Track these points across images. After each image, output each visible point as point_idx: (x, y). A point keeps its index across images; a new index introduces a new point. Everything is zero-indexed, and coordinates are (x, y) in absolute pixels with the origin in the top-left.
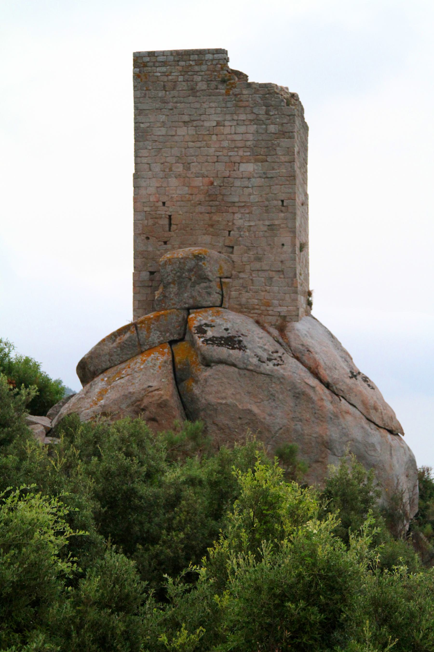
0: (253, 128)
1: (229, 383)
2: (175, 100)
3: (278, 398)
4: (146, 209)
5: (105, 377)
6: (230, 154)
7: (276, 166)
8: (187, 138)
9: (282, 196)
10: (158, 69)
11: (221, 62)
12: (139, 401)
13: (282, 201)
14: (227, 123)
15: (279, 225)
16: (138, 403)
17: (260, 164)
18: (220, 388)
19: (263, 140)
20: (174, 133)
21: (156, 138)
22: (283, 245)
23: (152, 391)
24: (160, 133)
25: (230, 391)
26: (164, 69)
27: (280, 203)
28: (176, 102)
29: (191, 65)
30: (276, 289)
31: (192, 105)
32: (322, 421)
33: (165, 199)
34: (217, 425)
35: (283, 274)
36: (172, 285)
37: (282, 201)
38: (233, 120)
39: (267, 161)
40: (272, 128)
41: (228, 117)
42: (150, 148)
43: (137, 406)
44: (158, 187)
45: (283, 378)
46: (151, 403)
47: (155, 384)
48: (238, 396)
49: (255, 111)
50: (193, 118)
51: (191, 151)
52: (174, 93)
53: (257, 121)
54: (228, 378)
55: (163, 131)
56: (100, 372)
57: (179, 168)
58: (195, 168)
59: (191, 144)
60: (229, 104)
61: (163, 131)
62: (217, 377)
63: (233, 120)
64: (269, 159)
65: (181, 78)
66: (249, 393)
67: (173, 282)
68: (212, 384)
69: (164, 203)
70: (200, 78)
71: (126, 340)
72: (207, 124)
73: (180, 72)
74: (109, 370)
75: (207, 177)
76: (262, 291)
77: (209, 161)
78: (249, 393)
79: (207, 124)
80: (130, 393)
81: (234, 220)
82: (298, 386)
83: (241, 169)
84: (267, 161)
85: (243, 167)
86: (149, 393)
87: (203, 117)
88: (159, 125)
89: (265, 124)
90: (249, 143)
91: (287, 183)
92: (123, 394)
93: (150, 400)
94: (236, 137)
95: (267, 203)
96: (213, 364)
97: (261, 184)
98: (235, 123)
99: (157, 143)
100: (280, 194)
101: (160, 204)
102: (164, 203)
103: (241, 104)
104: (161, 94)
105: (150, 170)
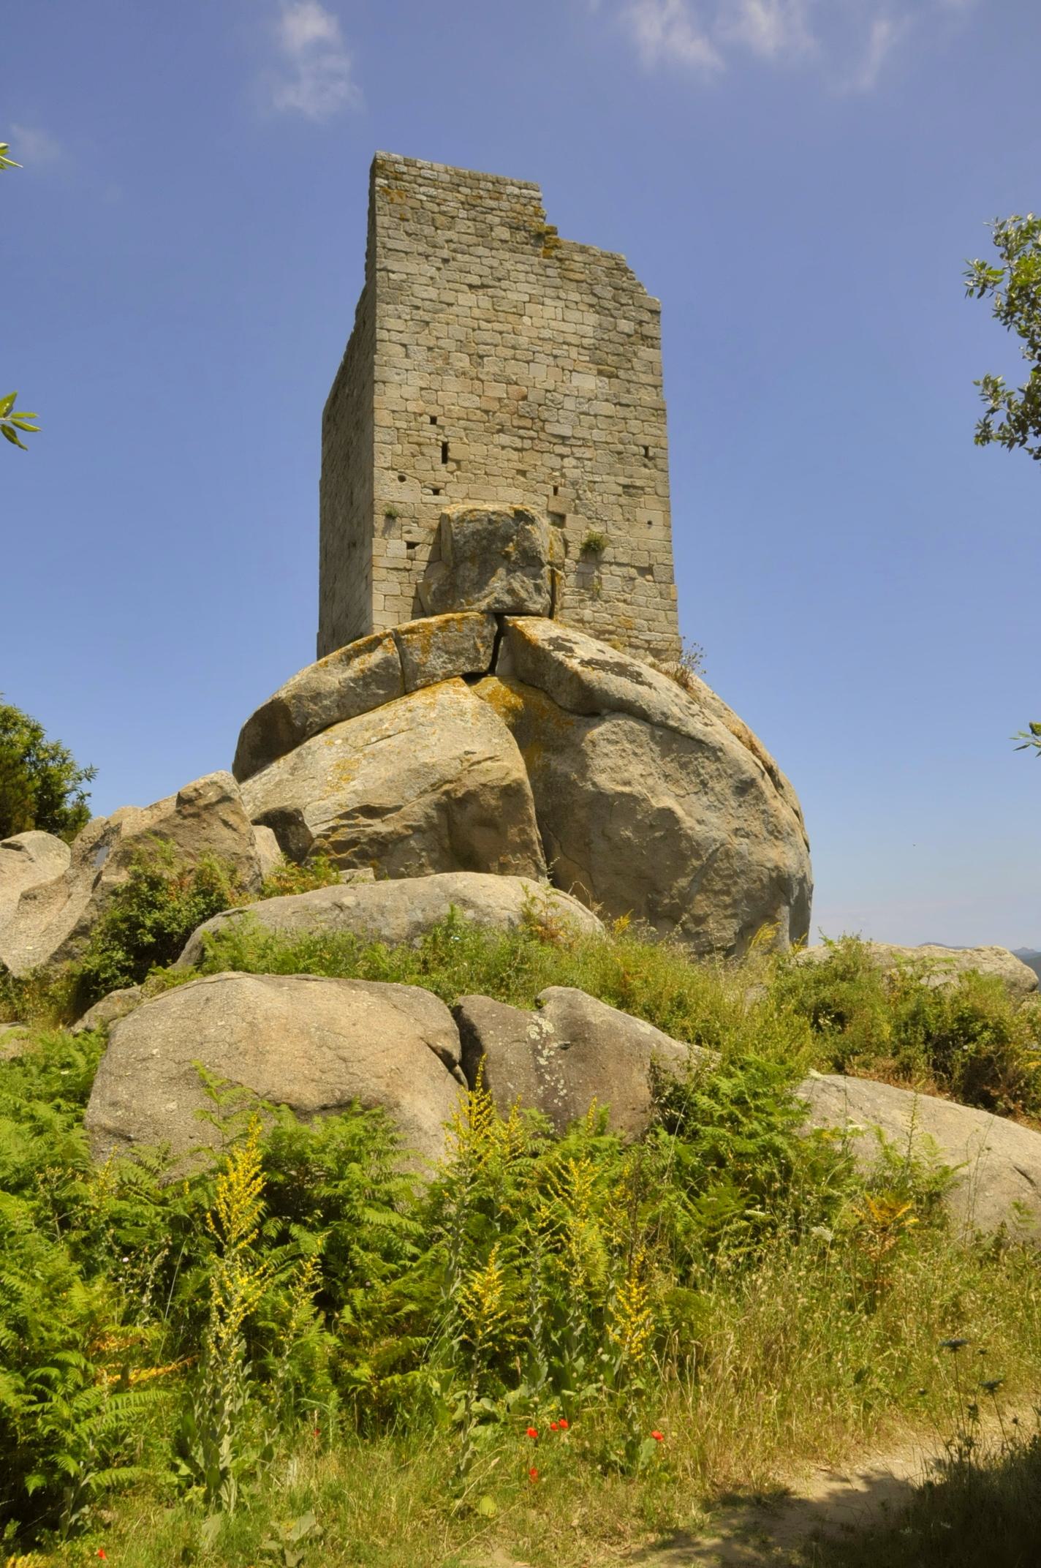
0: (592, 318)
1: (635, 754)
2: (453, 246)
3: (712, 789)
4: (398, 424)
5: (337, 737)
6: (555, 352)
7: (632, 387)
8: (476, 312)
9: (648, 441)
10: (422, 189)
11: (534, 203)
12: (451, 782)
13: (646, 448)
14: (547, 301)
15: (642, 488)
16: (447, 787)
17: (606, 380)
18: (620, 762)
19: (609, 341)
20: (452, 301)
21: (419, 303)
22: (650, 523)
23: (479, 762)
24: (425, 295)
25: (635, 770)
26: (432, 191)
27: (643, 451)
28: (454, 251)
29: (481, 198)
30: (642, 599)
31: (485, 261)
32: (776, 838)
33: (434, 411)
34: (609, 839)
35: (652, 574)
36: (469, 564)
37: (646, 448)
38: (558, 298)
39: (617, 377)
40: (625, 326)
41: (550, 292)
42: (408, 317)
43: (447, 793)
44: (422, 389)
45: (721, 750)
46: (484, 785)
47: (480, 749)
48: (650, 781)
49: (598, 289)
50: (486, 281)
51: (487, 336)
52: (450, 234)
53: (598, 309)
54: (632, 742)
55: (432, 293)
56: (317, 729)
57: (462, 361)
58: (491, 366)
59: (484, 325)
60: (550, 272)
61: (432, 293)
62: (614, 737)
63: (558, 298)
64: (621, 373)
65: (463, 214)
66: (666, 776)
67: (472, 559)
68: (605, 751)
69: (433, 420)
70: (497, 220)
71: (377, 666)
72: (512, 296)
73: (462, 203)
74: (336, 727)
75: (516, 383)
76: (618, 600)
77: (518, 357)
78: (666, 776)
79: (512, 296)
80: (425, 765)
81: (563, 467)
82: (745, 767)
83: (575, 383)
84: (617, 377)
85: (577, 380)
86: (473, 764)
87: (504, 284)
88: (424, 280)
89: (612, 316)
90: (586, 342)
91: (653, 419)
92: (406, 767)
93: (483, 780)
94: (564, 327)
95: (620, 447)
96: (605, 711)
97: (610, 414)
98: (561, 304)
99: (421, 312)
100: (641, 436)
101: (427, 419)
102: (433, 420)
103: (572, 275)
104: (428, 230)
105: (407, 356)
